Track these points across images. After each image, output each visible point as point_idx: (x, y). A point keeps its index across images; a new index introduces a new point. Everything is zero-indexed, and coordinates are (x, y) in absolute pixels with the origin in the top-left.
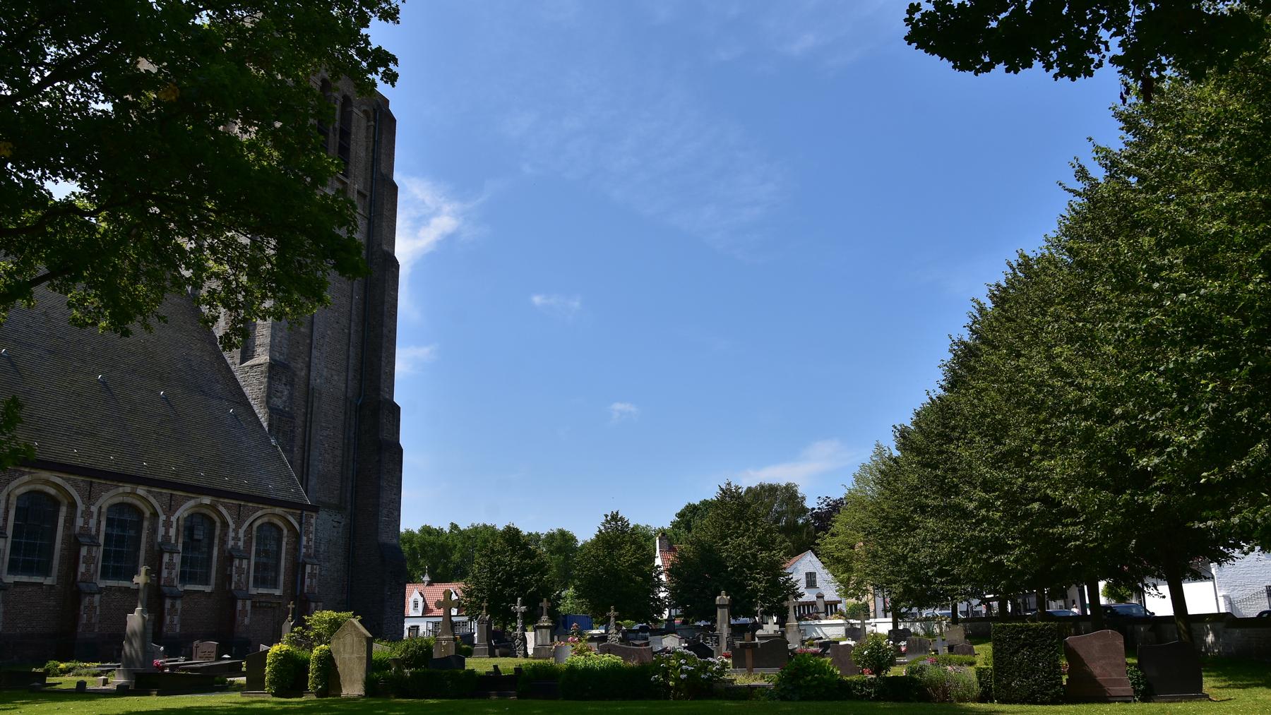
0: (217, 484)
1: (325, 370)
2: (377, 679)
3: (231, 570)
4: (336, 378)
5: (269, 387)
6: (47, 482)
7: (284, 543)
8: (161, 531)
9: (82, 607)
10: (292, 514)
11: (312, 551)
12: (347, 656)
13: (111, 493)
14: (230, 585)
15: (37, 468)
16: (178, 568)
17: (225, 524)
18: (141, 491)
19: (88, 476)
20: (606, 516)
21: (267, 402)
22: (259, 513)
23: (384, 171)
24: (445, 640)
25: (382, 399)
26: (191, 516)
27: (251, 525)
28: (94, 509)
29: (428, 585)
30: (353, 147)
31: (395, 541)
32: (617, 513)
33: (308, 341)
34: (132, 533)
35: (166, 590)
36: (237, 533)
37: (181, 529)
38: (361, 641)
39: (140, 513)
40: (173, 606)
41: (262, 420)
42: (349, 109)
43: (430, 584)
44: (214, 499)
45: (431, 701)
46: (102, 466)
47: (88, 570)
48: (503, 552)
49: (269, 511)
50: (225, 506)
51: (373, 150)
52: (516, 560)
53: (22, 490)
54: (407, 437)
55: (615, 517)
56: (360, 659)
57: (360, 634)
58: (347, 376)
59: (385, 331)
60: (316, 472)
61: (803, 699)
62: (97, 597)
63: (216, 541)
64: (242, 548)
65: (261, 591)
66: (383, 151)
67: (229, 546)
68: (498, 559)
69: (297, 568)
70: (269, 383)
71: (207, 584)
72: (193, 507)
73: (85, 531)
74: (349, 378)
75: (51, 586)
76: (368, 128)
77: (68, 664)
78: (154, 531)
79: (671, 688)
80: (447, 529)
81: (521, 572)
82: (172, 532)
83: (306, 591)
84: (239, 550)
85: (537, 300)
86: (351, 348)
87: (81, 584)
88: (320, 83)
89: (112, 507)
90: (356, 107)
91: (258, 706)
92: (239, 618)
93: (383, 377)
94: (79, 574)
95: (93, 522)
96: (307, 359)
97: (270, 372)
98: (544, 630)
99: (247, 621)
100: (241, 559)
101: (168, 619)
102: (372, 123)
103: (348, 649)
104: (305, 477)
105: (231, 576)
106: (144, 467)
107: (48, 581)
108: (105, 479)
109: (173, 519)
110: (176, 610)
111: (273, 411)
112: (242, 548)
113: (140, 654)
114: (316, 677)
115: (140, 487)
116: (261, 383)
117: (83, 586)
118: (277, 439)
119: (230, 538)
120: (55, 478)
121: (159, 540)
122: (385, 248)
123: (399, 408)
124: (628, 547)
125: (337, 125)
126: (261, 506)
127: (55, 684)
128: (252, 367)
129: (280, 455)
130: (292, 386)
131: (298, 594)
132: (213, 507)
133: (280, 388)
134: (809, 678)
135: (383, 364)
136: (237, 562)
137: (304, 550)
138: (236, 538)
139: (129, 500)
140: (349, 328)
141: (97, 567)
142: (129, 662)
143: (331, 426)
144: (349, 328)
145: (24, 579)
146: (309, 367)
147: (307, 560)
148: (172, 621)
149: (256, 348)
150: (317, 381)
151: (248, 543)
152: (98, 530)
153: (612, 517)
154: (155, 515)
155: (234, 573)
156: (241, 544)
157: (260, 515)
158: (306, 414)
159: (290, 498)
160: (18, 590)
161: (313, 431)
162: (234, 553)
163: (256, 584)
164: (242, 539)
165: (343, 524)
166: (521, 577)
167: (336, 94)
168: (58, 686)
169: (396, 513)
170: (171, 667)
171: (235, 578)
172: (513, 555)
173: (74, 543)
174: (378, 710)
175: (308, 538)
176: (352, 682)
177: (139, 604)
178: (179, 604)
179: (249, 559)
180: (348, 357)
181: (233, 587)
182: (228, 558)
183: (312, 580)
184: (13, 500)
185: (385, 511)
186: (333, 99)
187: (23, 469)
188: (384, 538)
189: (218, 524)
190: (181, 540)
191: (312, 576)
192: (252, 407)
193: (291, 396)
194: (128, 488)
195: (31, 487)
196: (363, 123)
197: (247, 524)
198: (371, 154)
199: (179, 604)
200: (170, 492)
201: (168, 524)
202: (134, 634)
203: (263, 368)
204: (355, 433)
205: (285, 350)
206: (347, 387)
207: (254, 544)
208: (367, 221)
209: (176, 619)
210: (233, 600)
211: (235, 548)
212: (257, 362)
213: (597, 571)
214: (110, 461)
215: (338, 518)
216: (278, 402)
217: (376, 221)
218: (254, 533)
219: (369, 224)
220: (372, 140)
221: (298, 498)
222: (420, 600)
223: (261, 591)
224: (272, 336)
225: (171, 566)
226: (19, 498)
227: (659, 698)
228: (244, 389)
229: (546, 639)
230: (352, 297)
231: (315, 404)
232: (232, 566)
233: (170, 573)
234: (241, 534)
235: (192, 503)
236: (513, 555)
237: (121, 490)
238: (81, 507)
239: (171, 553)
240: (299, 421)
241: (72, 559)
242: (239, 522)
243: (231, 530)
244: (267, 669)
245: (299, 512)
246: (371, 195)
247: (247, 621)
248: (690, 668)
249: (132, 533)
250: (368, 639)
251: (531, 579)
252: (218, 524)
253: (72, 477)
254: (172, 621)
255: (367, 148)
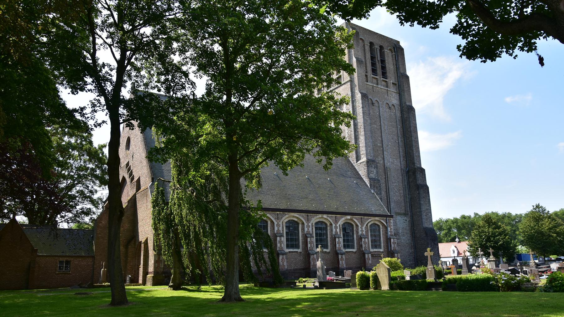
0: (352, 211)
1: (391, 159)
2: (393, 283)
3: (362, 243)
4: (396, 161)
5: (368, 170)
6: (294, 217)
7: (381, 231)
8: (334, 230)
9: (311, 259)
10: (383, 219)
11: (393, 233)
12: (382, 275)
13: (315, 218)
14: (362, 248)
15: (290, 212)
16: (342, 244)
17: (357, 226)
18: (325, 216)
19: (306, 213)
20: (533, 206)
21: (368, 176)
22: (369, 220)
23: (402, 72)
24: (430, 268)
25: (416, 167)
26: (344, 224)
27: (367, 225)
28: (310, 224)
29: (458, 243)
30: (387, 65)
31: (431, 226)
32: (539, 204)
33: (382, 149)
34: (325, 232)
35: (338, 251)
36: (362, 229)
37: (341, 229)
38: (386, 270)
39: (326, 224)
40: (342, 257)
41: (367, 183)
42: (383, 51)
43: (459, 242)
44: (351, 216)
45: (407, 291)
46: (310, 209)
47: (311, 246)
48: (484, 226)
49: (373, 219)
50: (356, 219)
51: (396, 65)
52: (491, 230)
53: (287, 220)
54: (430, 182)
55: (538, 206)
56: (386, 276)
57: (385, 267)
58: (400, 160)
59: (413, 139)
60: (393, 201)
61: (554, 291)
62: (315, 255)
63: (355, 232)
64: (365, 234)
65: (375, 250)
66: (400, 63)
67: (360, 234)
68: (482, 230)
69: (388, 240)
70: (368, 168)
71: (354, 249)
72: (344, 220)
73: (308, 233)
74: (401, 161)
75: (301, 252)
76: (392, 56)
77: (306, 279)
78: (332, 230)
79: (500, 287)
80: (473, 216)
81: (494, 235)
82: (338, 230)
83: (392, 249)
84: (363, 235)
85: (508, 100)
86: (400, 148)
87: (309, 251)
88: (369, 44)
89: (316, 223)
90: (386, 49)
91: (351, 292)
92: (367, 261)
93: (415, 158)
94: (308, 247)
95: (310, 229)
96: (382, 156)
97: (367, 164)
98: (492, 262)
99: (370, 262)
100: (365, 238)
101: (341, 262)
102: (394, 53)
103: (382, 273)
104: (389, 203)
105: (362, 245)
106: (325, 208)
107: (299, 250)
108: (314, 214)
109: (338, 225)
110: (343, 259)
111: (370, 179)
112: (365, 234)
113: (322, 275)
114: (373, 283)
115: (324, 215)
116: (365, 169)
117: (310, 252)
118: (374, 190)
119: (360, 231)
120: (296, 215)
121: (334, 234)
122: (408, 104)
123: (424, 170)
124: (546, 220)
125: (379, 59)
126: (370, 217)
127: (299, 286)
128: (361, 163)
129: (376, 196)
130: (377, 168)
131: (390, 250)
132: (351, 219)
133: (373, 169)
134: (557, 282)
135: (414, 152)
136: (363, 240)
137: (389, 233)
138: (362, 231)
139: (321, 220)
140: (398, 140)
141: (314, 244)
142: (319, 278)
143: (397, 181)
144: (398, 140)
145: (291, 250)
146: (384, 159)
147: (391, 237)
148: (342, 263)
149: (361, 156)
150: (388, 164)
151: (367, 232)
152: (313, 232)
153: (537, 206)
154: (331, 224)
155: (363, 244)
156: (364, 232)
157: (371, 221)
158: (385, 178)
159: (381, 213)
160: (290, 254)
161: (389, 185)
162: (362, 236)
163: (372, 248)
164: (364, 231)
165: (408, 221)
166: (494, 237)
167: (376, 47)
168: (300, 286)
169: (430, 214)
170: (336, 280)
171: (364, 246)
172: (489, 227)
173: (305, 237)
174: (244, 287)
175: (391, 228)
176: (385, 285)
177: (320, 258)
178: (344, 256)
179: (368, 238)
180: (400, 152)
181: (363, 249)
182: (360, 238)
183: (394, 245)
184: (284, 224)
185: (425, 214)
186: (375, 49)
187: (285, 213)
188: (426, 225)
189: (355, 226)
190: (342, 233)
191: (394, 243)
192: (363, 179)
193: (377, 172)
194: (320, 216)
195: (289, 219)
196: (390, 54)
197: (365, 225)
198: (395, 66)
199: (344, 256)
200: (335, 215)
201: (336, 228)
202: (319, 268)
203: (365, 163)
204: (407, 183)
205: (372, 155)
206: (401, 165)
207: (369, 232)
208: (398, 94)
209: (344, 262)
210: (364, 254)
211: (362, 234)
212: (362, 161)
213: (531, 232)
214: (313, 207)
215: (405, 218)
216: (372, 176)
217: (402, 93)
218: (369, 228)
219: (399, 95)
220: (395, 60)
221: (384, 213)
222: (455, 249)
223: (375, 250)
224: (366, 150)
225: (339, 243)
226: (286, 223)
227: (495, 291)
228: (359, 172)
229: (493, 266)
230: (397, 127)
231: (389, 174)
232: (361, 241)
233: (339, 245)
234: (364, 229)
235: (343, 219)
236: (489, 227)
237: (318, 217)
238: (306, 224)
239: (339, 238)
240: (383, 181)
241: (306, 243)
242: (362, 224)
243: (359, 228)
244: (357, 280)
245: (386, 218)
246: (398, 83)
247: (370, 262)
248: (505, 279)
249: (325, 232)
250: (388, 269)
251: (500, 238)
252: (355, 226)
253: (301, 214)
254: (342, 263)
255: (393, 64)
